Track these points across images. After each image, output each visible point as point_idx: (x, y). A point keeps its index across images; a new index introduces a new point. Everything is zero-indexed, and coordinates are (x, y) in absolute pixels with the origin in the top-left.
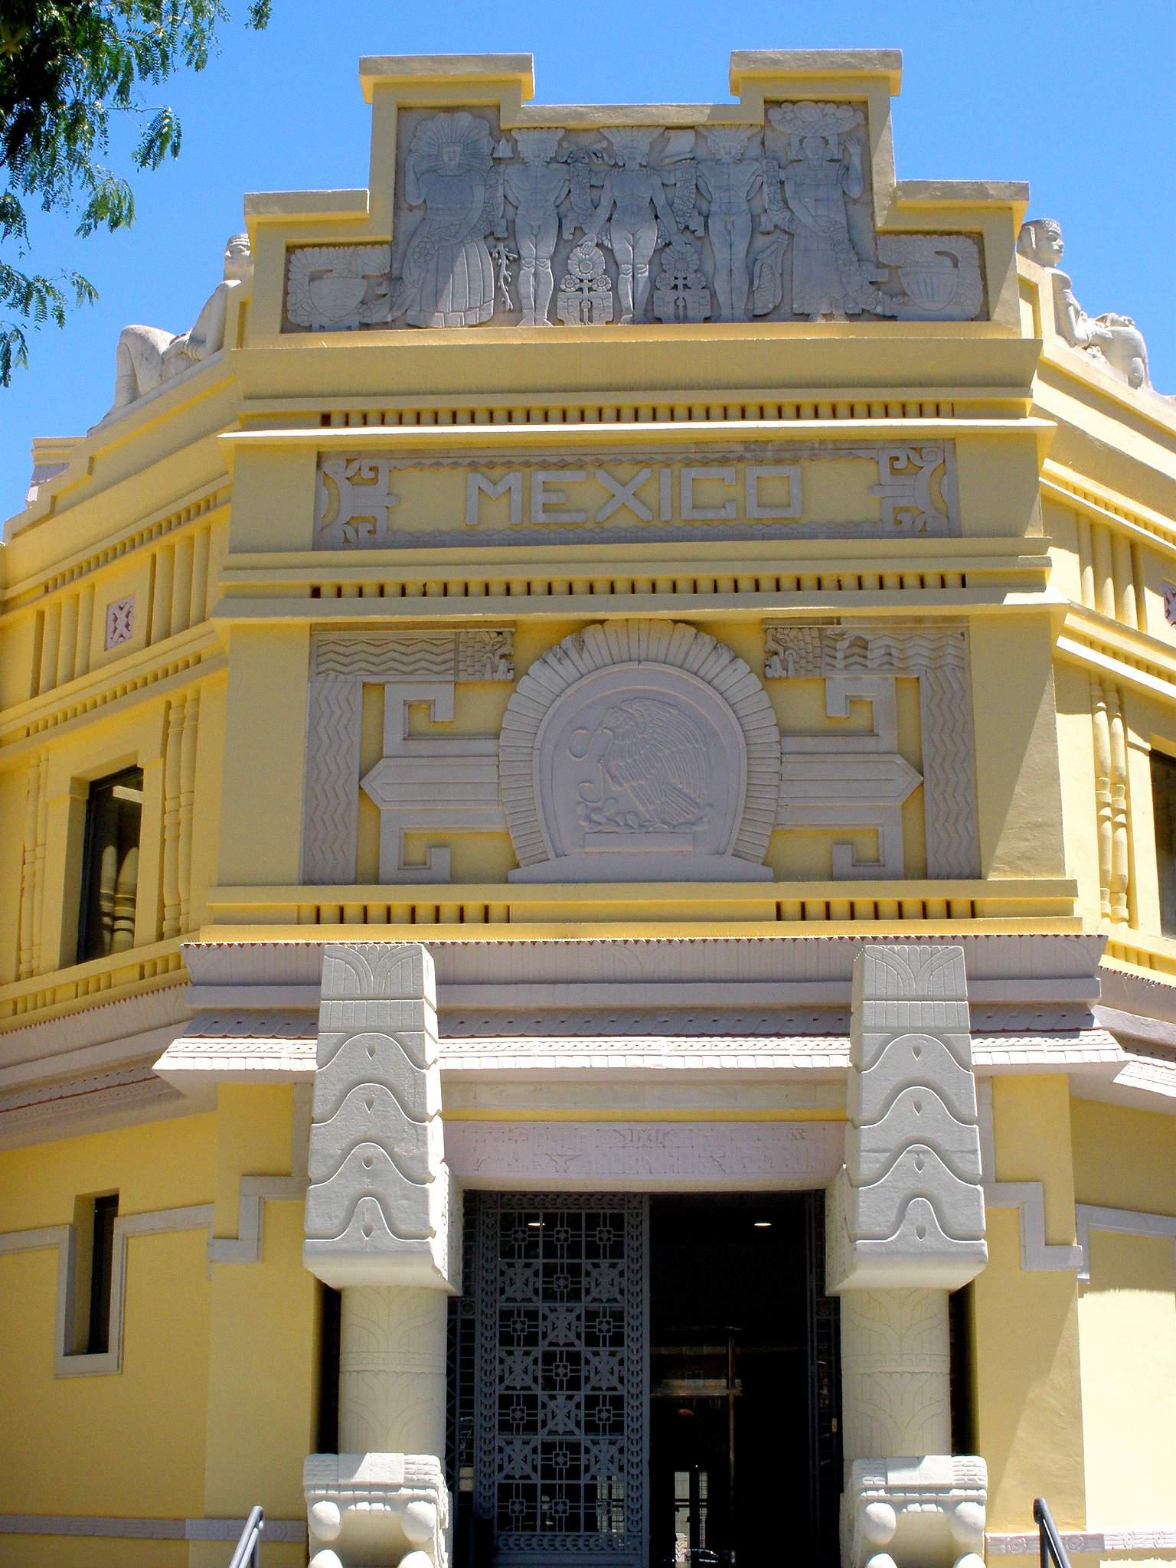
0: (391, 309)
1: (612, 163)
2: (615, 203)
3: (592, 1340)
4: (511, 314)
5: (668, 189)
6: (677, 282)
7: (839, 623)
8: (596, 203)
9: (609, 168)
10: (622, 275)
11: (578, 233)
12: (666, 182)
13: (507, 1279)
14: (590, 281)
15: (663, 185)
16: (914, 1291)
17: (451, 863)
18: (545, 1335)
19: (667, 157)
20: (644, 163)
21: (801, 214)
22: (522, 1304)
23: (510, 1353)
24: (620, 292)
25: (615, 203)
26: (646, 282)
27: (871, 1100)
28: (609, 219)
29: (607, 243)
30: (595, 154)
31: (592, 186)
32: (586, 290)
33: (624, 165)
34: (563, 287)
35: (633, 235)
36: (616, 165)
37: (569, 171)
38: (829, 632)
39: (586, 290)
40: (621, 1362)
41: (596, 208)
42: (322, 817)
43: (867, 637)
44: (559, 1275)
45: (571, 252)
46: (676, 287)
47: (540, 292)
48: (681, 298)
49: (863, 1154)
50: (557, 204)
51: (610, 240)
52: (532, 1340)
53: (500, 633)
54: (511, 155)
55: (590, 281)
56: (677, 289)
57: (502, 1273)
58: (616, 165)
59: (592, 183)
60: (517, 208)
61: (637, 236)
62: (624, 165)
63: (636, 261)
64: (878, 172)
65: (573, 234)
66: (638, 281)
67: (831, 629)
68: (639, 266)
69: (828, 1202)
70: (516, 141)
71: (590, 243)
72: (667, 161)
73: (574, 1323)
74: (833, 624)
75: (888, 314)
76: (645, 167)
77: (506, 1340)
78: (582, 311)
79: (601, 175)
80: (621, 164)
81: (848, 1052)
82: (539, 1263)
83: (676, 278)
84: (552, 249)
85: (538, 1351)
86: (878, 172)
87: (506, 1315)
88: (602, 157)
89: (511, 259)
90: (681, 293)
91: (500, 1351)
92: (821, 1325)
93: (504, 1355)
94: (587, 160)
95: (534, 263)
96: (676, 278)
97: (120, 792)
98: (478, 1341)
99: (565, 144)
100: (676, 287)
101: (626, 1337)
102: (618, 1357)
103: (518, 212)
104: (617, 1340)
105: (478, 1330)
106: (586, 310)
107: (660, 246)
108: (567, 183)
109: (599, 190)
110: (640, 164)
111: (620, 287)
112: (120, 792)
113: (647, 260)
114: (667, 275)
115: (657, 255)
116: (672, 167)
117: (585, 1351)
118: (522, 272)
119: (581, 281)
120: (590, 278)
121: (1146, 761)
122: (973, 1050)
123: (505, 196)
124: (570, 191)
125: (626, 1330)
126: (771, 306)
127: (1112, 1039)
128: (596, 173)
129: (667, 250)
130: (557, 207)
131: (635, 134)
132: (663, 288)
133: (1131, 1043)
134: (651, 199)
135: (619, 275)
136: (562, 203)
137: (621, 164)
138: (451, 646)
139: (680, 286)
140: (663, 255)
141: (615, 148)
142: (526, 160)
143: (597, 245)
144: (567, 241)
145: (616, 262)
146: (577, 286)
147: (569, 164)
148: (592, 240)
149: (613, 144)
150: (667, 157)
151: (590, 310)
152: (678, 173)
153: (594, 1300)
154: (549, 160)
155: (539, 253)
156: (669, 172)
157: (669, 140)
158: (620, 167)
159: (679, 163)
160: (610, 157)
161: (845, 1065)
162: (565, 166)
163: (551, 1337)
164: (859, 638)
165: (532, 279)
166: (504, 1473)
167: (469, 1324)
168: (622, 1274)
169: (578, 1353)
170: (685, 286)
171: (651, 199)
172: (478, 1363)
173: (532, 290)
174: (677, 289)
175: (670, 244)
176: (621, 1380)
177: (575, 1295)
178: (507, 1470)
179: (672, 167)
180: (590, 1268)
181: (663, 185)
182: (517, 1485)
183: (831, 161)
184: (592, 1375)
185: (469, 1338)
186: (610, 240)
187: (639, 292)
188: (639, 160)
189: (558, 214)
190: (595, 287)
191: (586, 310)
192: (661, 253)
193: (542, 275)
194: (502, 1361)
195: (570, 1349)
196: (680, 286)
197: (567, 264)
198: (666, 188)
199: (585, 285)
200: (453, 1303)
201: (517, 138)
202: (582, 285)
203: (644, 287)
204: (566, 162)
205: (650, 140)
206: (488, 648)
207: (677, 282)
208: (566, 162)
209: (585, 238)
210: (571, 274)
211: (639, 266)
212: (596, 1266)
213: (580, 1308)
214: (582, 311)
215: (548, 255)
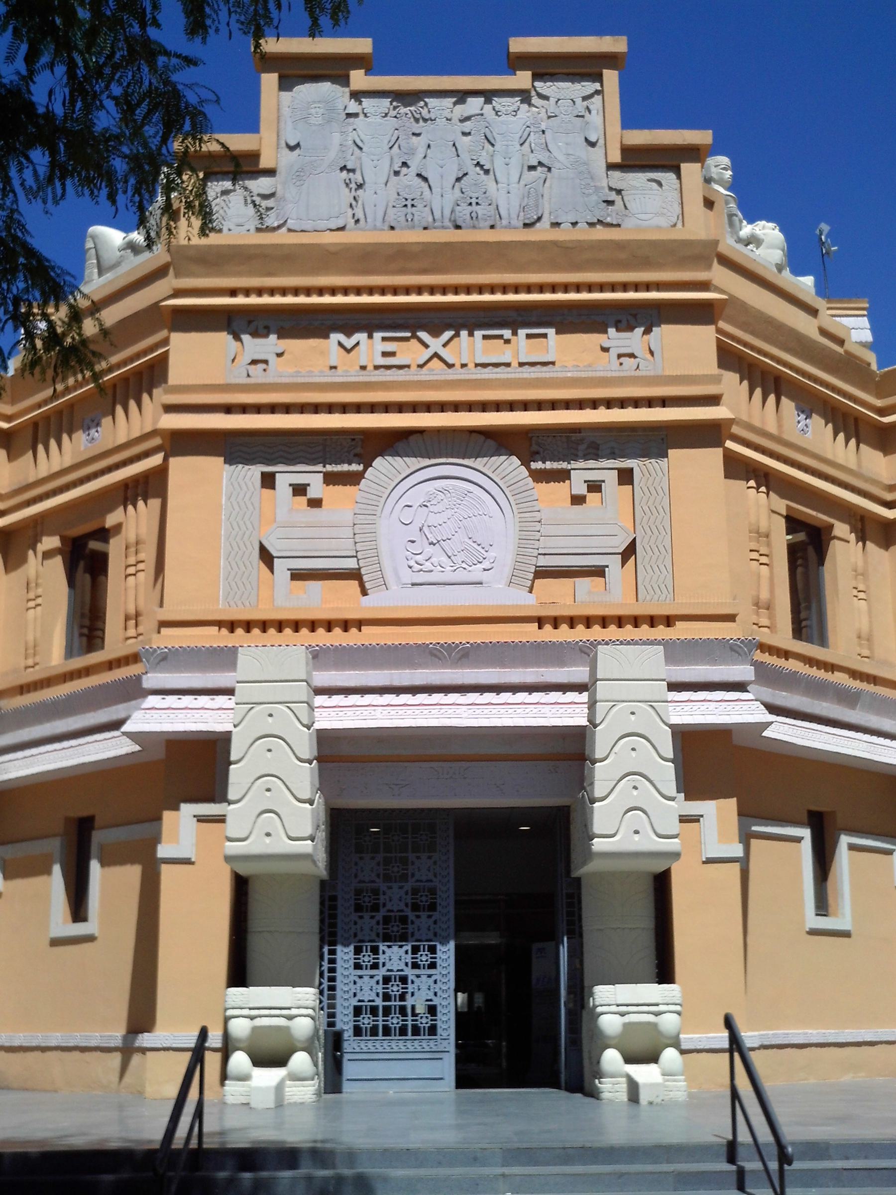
0: (277, 218)
3: (415, 907)
7: (580, 432)
13: (358, 927)
16: (629, 874)
17: (259, 932)
18: (384, 905)
21: (556, 153)
22: (369, 885)
23: (361, 917)
27: (600, 745)
28: (425, 157)
38: (573, 439)
39: (409, 206)
40: (435, 922)
42: (254, 508)
43: (598, 442)
44: (393, 1015)
46: (470, 204)
52: (375, 908)
53: (353, 440)
57: (356, 864)
67: (575, 436)
69: (573, 815)
73: (404, 896)
74: (576, 433)
75: (615, 223)
77: (358, 908)
81: (586, 715)
82: (380, 857)
85: (379, 916)
87: (358, 892)
90: (474, 207)
91: (354, 916)
92: (570, 896)
93: (357, 919)
97: (93, 545)
98: (340, 910)
100: (470, 204)
101: (438, 905)
102: (433, 918)
104: (432, 907)
105: (340, 902)
112: (93, 545)
117: (411, 916)
121: (783, 521)
122: (670, 714)
125: (438, 901)
126: (535, 217)
127: (762, 707)
133: (773, 709)
138: (321, 448)
139: (474, 204)
146: (404, 204)
153: (417, 881)
161: (584, 724)
163: (389, 906)
164: (593, 442)
166: (358, 938)
167: (333, 898)
168: (435, 863)
169: (407, 917)
170: (477, 204)
172: (340, 924)
176: (436, 994)
177: (404, 878)
178: (359, 997)
180: (414, 918)
182: (366, 1006)
183: (577, 116)
184: (416, 932)
185: (334, 908)
194: (356, 864)
195: (401, 914)
196: (474, 204)
199: (409, 203)
200: (323, 883)
206: (346, 449)
212: (418, 858)
213: (408, 886)
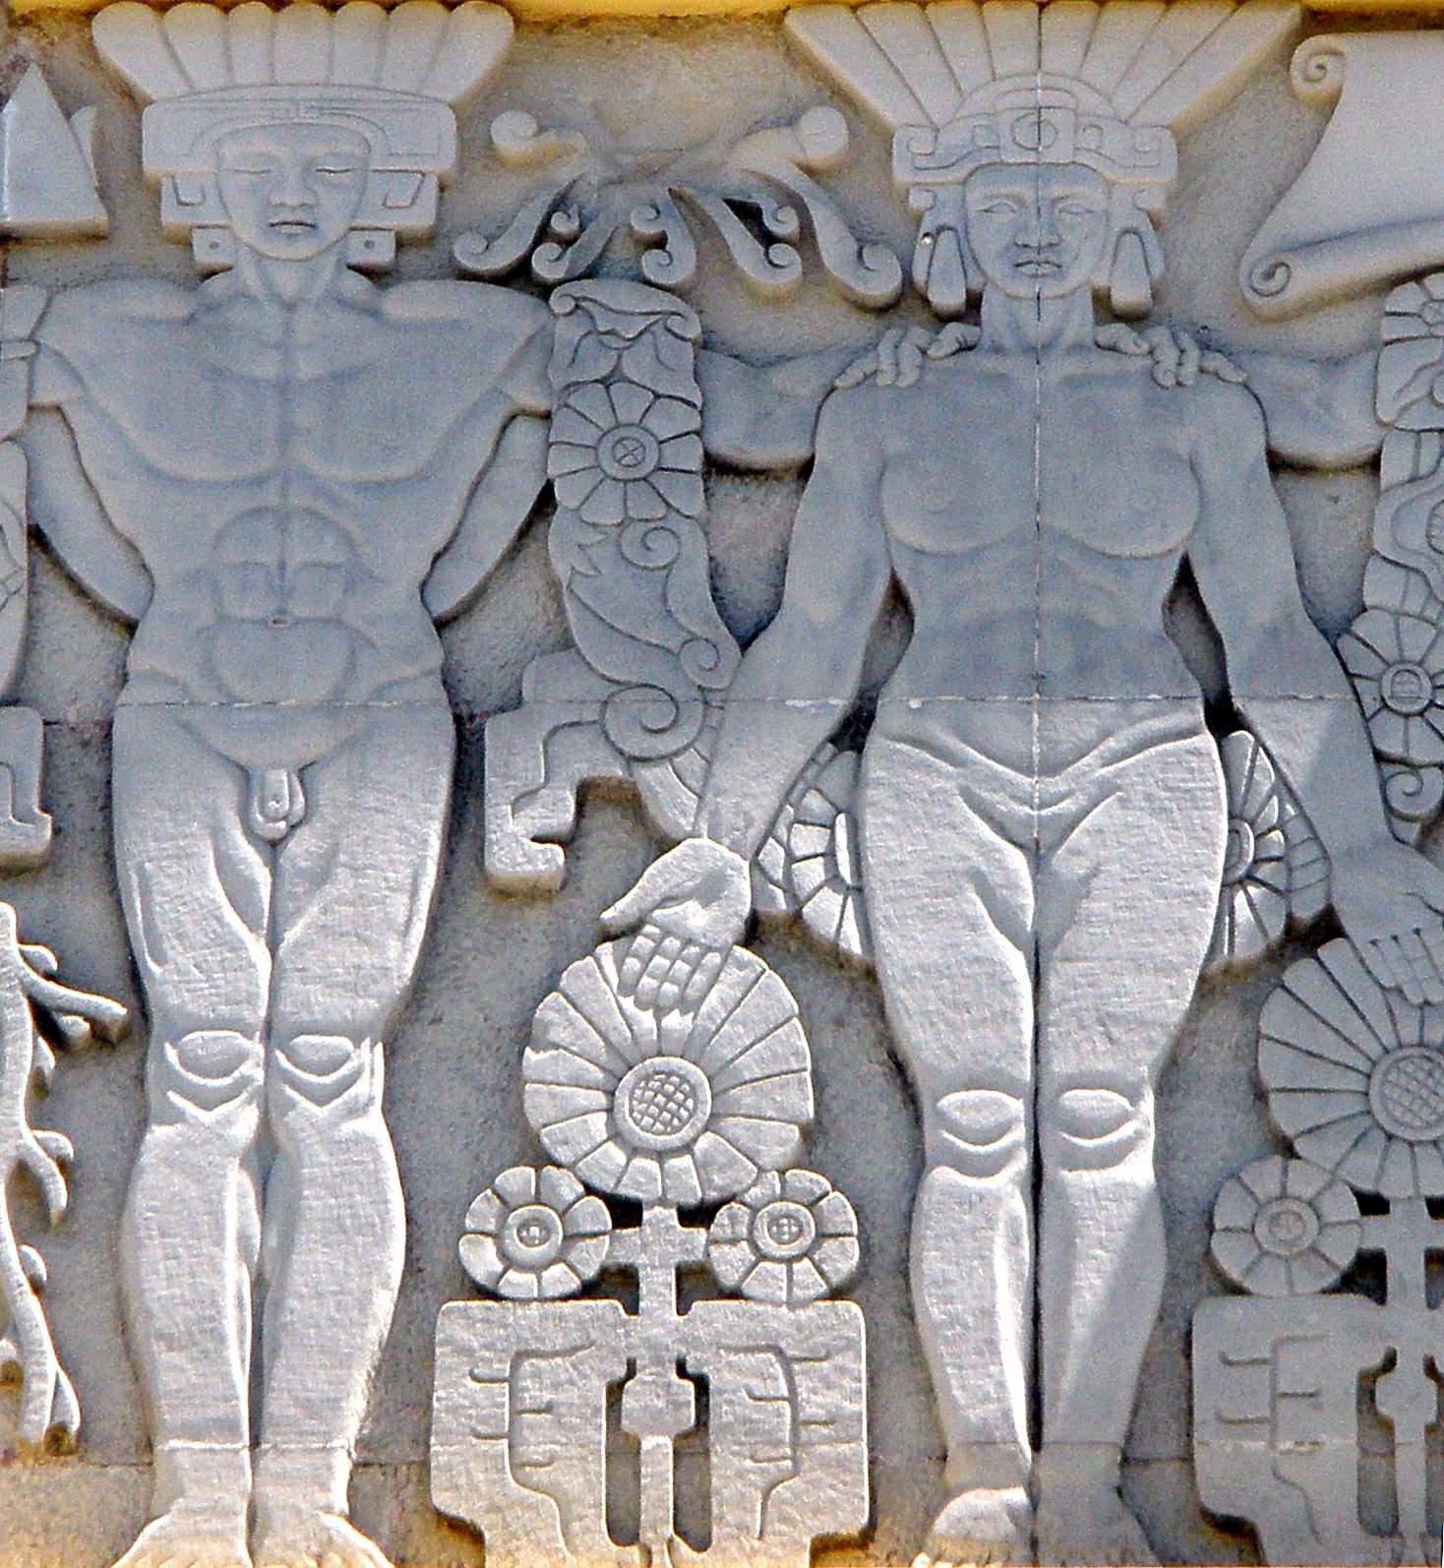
1: (882, 284)
2: (898, 600)
4: (66, 1472)
5: (1308, 494)
6: (1377, 1234)
8: (750, 593)
9: (860, 328)
10: (943, 1176)
11: (608, 829)
12: (1295, 443)
14: (697, 1215)
15: (1278, 464)
19: (1313, 245)
20: (1128, 294)
24: (931, 1308)
25: (898, 600)
26: (1141, 1222)
29: (828, 913)
30: (748, 213)
31: (717, 467)
32: (658, 1286)
33: (974, 302)
34: (481, 1260)
35: (1037, 857)
36: (909, 299)
37: (542, 344)
39: (658, 1286)
41: (745, 644)
45: (551, 985)
47: (297, 1307)
48: (1409, 1367)
49: (526, 1416)
50: (445, 603)
51: (858, 891)
54: (90, 213)
55: (697, 1215)
56: (1378, 1292)
58: (909, 299)
59: (725, 443)
60: (130, 627)
61: (1067, 864)
62: (974, 302)
63: (1060, 1065)
64: (1202, 1443)
65: (567, 842)
66: (1069, 1217)
68: (1078, 1100)
70: (133, 101)
71: (695, 917)
72: (1308, 278)
76: (1135, 319)
78: (624, 1451)
79: (800, 382)
80: (948, 296)
83: (1373, 1204)
84: (403, 959)
86: (1202, 1443)
88: (805, 240)
89: (76, 1027)
94: (680, 263)
95: (253, 1070)
96: (1373, 1204)
99: (512, 134)
103: (139, 660)
106: (657, 1446)
107: (1247, 947)
108: (525, 435)
109: (778, 497)
110: (1104, 307)
111: (932, 1262)
113: (1144, 1063)
114: (1303, 1181)
115: (1225, 1019)
116: (1344, 327)
118: (159, 1134)
119: (626, 1212)
120: (693, 1193)
123: (37, 537)
124: (546, 502)
128: (758, 364)
129: (1301, 975)
130: (442, 625)
131: (1062, 55)
132: (1267, 1283)
134: (1186, 579)
135: (919, 1167)
136: (479, 594)
137: (948, 296)
140: (1276, 1017)
141: (902, 174)
142: (203, 257)
143: (754, 933)
144: (532, 893)
145: (899, 1067)
146: (592, 1258)
147: (544, 291)
148: (710, 890)
149: (887, 137)
150: (1313, 245)
151: (692, 1445)
152: (1397, 374)
154: (383, 254)
155: (293, 985)
156: (1333, 363)
157: (1329, 105)
158: (943, 319)
159: (1407, 298)
160: (864, 241)
162: (510, 308)
165: (238, 1188)
171: (1186, 579)
173: (235, 1278)
174: (1378, 1292)
175: (1327, 927)
179: (1344, 327)
181: (1278, 464)
186: (858, 891)
187: (1080, 1331)
188: (1086, 270)
189: (449, 681)
190: (729, 1263)
191: (657, 1446)
192: (1252, 1008)
193: (316, 1162)
197: (513, 1079)
198: (1287, 480)
201: (145, 83)
202: (639, 1248)
203: (1120, 1293)
204: (518, 276)
205: (1181, 105)
207: (1377, 1234)
208: (518, 276)
209: (660, 874)
210: (542, 1159)
211: (1078, 1100)
214: (624, 1451)
215: (369, 1006)
